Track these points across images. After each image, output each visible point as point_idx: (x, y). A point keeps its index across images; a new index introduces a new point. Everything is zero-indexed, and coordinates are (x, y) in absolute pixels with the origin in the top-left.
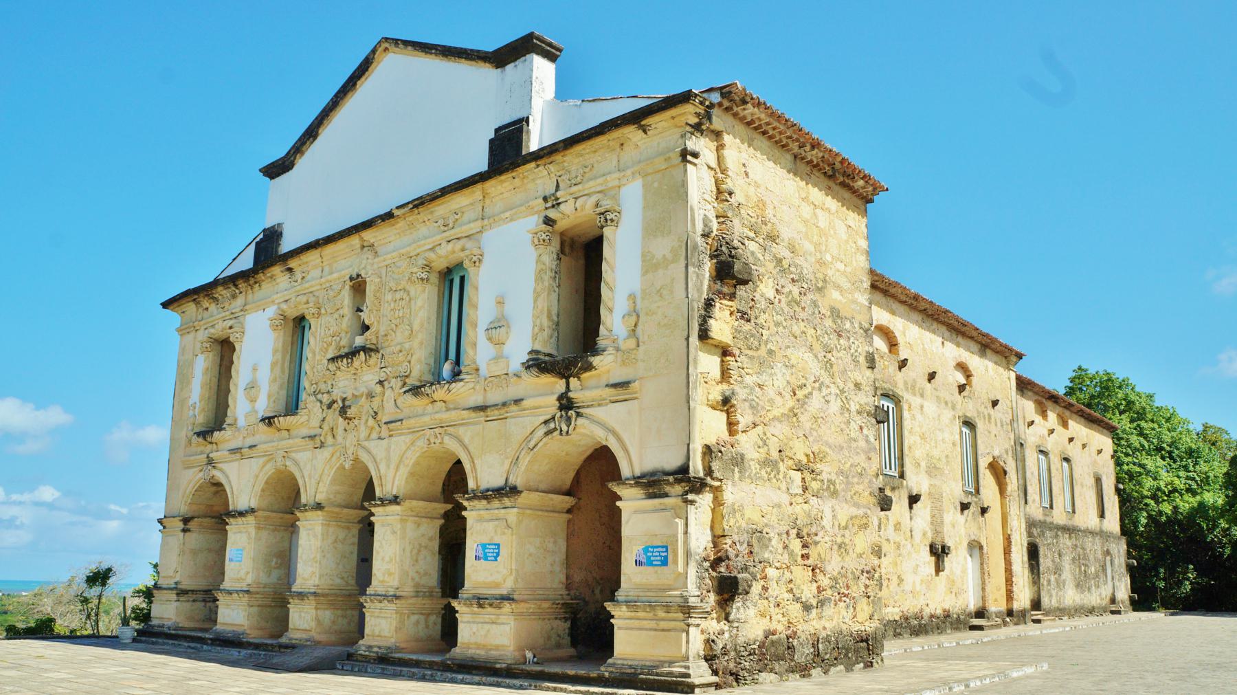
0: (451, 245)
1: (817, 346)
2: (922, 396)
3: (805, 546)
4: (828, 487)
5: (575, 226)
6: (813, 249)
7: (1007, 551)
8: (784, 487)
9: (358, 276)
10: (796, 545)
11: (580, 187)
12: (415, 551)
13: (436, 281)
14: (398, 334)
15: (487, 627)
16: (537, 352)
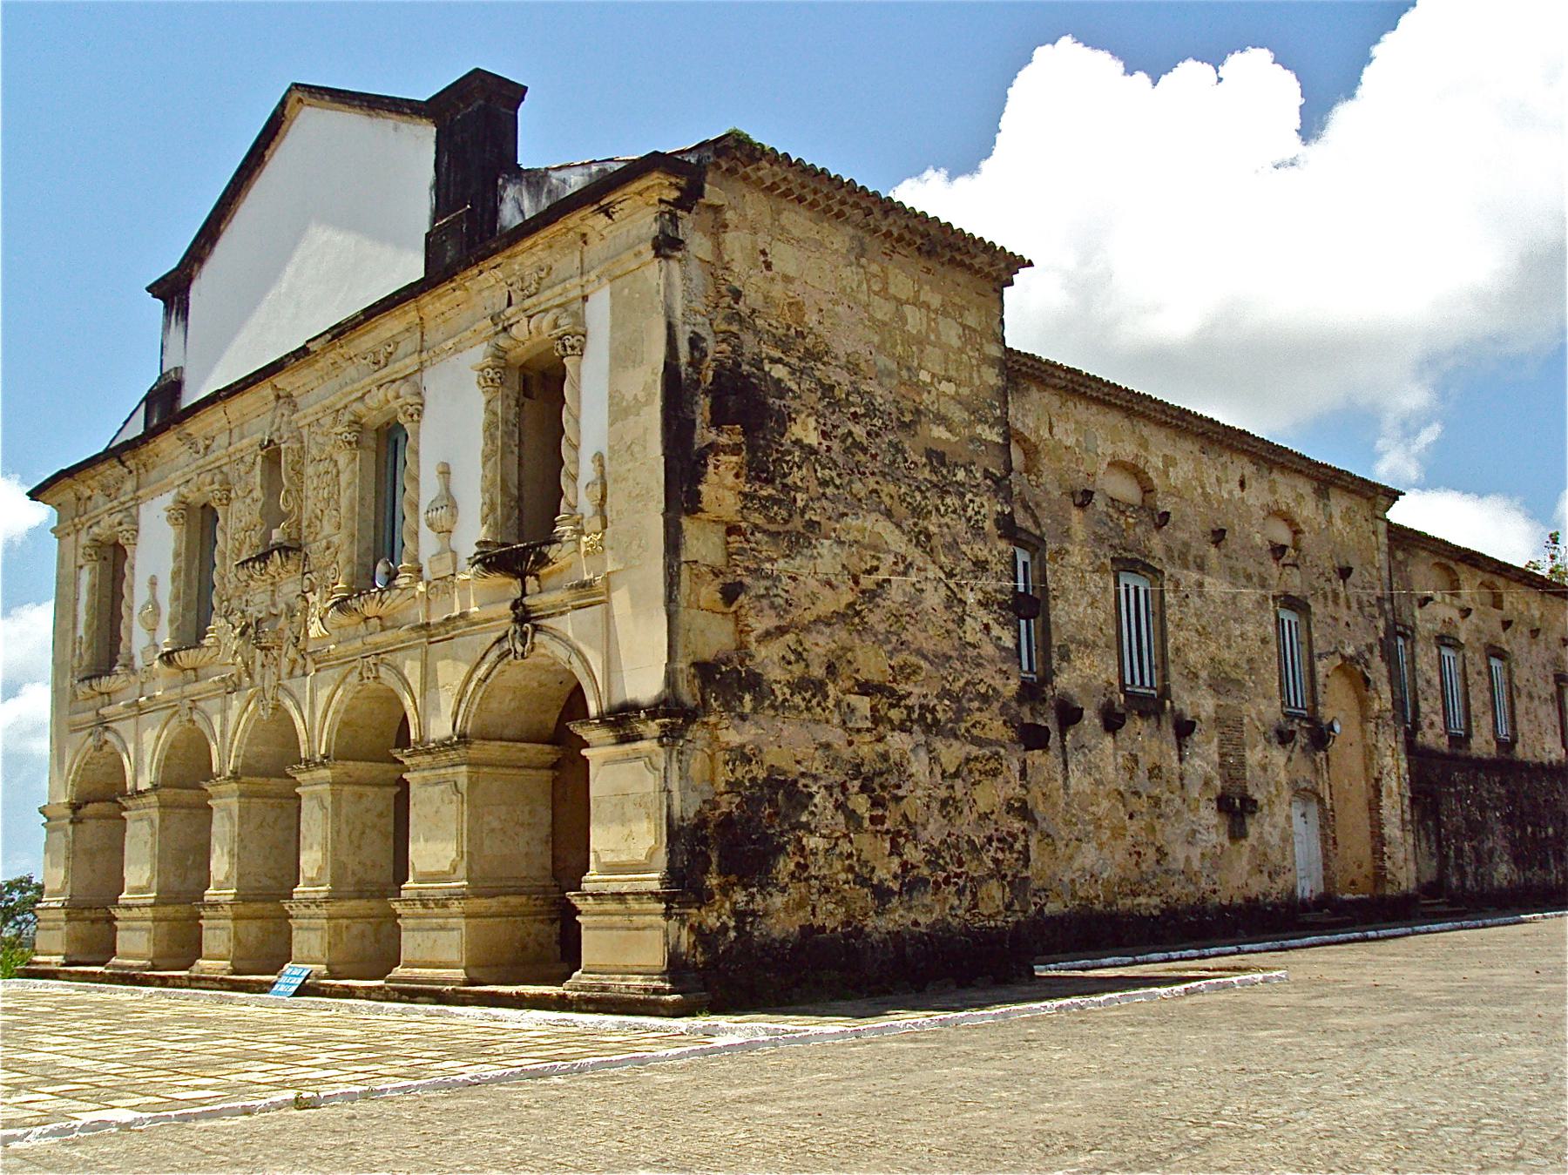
0: (382, 390)
1: (901, 510)
2: (1201, 568)
3: (876, 803)
4: (922, 717)
5: (534, 353)
6: (894, 367)
7: (1374, 806)
8: (836, 720)
9: (270, 441)
10: (861, 804)
11: (534, 300)
12: (357, 833)
13: (373, 444)
14: (325, 522)
15: (433, 934)
16: (486, 543)
